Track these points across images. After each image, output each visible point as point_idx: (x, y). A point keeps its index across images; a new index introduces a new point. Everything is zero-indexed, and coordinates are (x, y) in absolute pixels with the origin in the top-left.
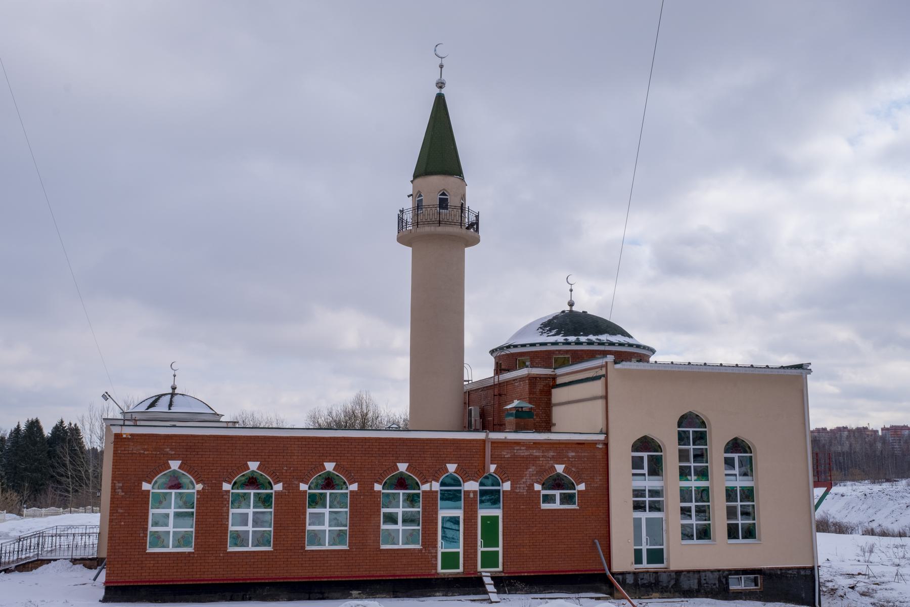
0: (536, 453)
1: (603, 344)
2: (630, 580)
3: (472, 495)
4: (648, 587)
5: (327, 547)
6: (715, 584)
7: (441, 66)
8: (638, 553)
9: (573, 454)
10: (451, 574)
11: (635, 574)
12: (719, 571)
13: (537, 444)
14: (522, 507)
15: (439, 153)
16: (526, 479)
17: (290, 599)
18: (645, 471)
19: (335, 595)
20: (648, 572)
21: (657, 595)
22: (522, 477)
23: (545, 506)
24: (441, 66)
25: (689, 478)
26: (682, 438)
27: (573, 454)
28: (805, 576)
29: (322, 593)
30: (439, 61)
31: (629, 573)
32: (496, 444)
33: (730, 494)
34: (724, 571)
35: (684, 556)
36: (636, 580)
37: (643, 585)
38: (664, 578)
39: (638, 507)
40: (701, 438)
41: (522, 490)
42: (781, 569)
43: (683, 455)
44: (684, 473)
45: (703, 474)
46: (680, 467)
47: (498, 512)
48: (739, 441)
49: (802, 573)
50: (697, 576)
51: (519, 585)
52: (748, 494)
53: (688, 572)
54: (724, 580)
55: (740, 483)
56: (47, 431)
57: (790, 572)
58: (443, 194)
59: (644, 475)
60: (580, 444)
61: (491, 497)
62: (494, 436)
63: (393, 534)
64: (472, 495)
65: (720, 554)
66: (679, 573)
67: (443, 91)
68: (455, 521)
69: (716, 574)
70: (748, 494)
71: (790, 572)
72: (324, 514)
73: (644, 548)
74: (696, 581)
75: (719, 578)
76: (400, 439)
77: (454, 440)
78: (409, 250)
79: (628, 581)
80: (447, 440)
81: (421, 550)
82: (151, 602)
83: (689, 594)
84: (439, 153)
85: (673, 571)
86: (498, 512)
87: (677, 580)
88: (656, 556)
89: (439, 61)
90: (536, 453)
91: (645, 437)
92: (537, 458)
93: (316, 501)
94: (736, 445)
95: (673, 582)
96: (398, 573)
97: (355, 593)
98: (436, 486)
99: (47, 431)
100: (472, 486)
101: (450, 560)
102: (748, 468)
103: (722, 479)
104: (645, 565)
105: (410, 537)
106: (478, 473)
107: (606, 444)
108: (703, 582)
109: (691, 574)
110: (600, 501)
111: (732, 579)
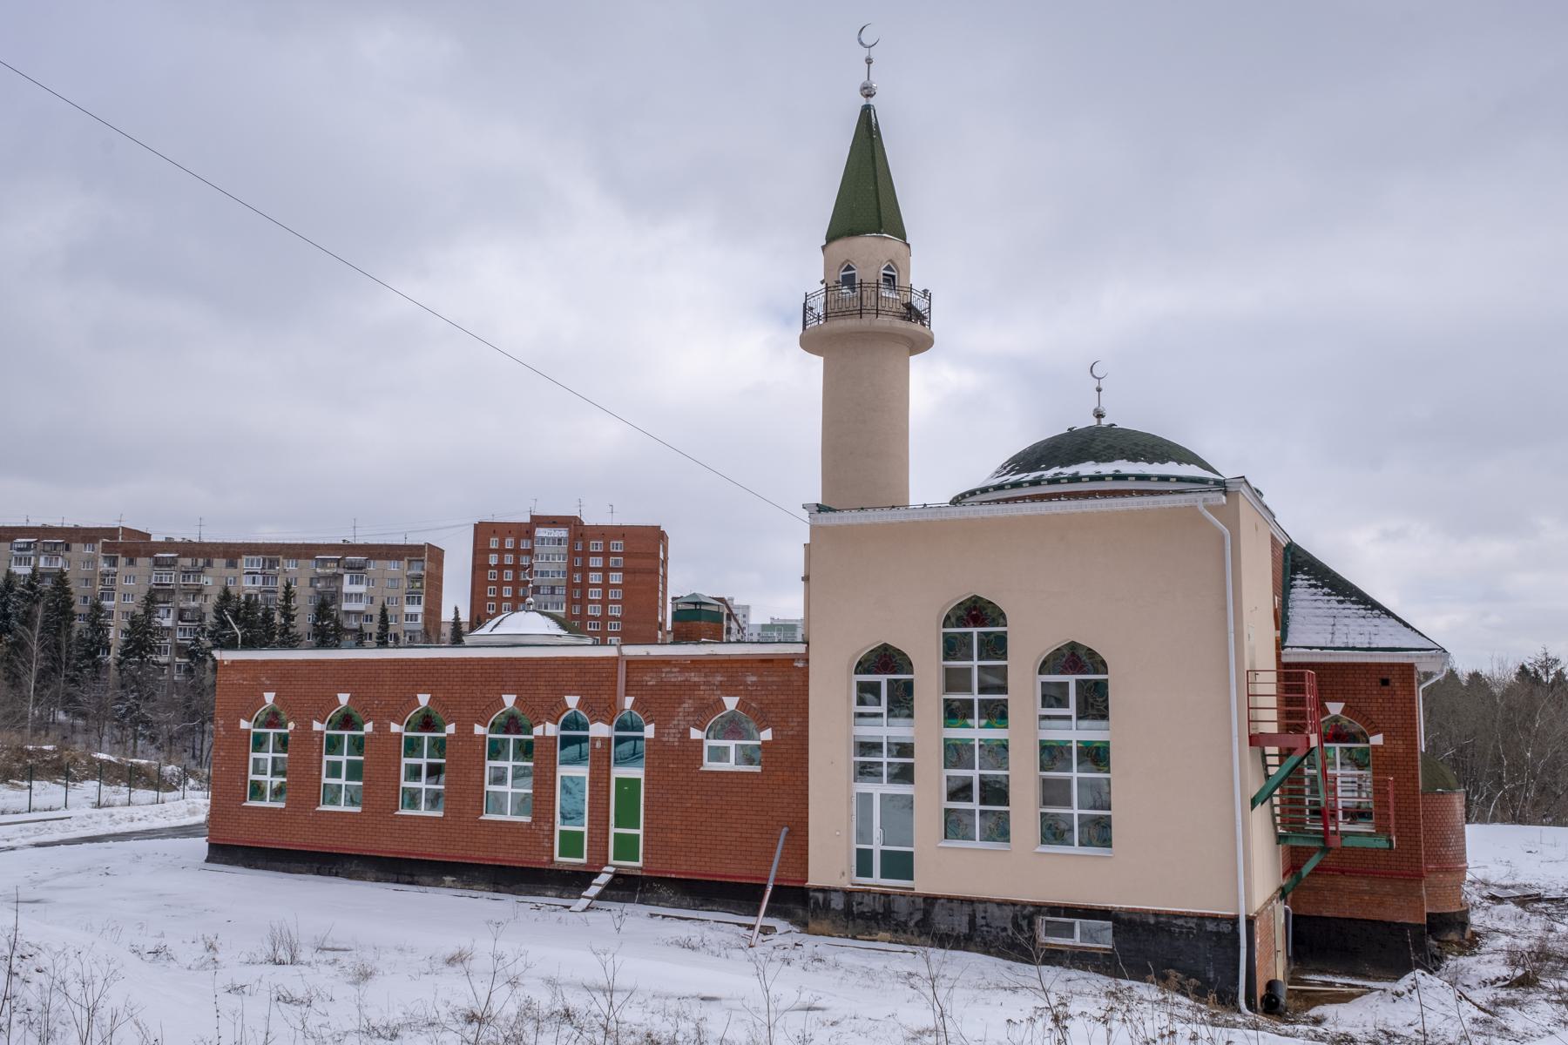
0: (694, 678)
1: (1124, 477)
2: (837, 903)
3: (598, 745)
4: (869, 919)
5: (508, 817)
6: (1005, 929)
7: (869, 61)
8: (864, 859)
9: (754, 679)
10: (569, 864)
11: (848, 894)
12: (1014, 904)
13: (696, 663)
14: (674, 762)
15: (867, 201)
16: (679, 720)
17: (377, 880)
18: (1072, 710)
19: (278, 864)
20: (869, 892)
21: (887, 935)
22: (672, 717)
23: (709, 765)
24: (869, 61)
25: (969, 721)
26: (953, 647)
27: (754, 679)
28: (1218, 934)
29: (412, 875)
30: (864, 53)
31: (835, 890)
32: (632, 663)
33: (1052, 754)
34: (1024, 905)
35: (950, 869)
36: (848, 905)
37: (862, 915)
38: (901, 907)
39: (865, 772)
40: (996, 646)
41: (672, 739)
42: (1157, 914)
43: (954, 680)
44: (955, 713)
45: (997, 713)
46: (946, 700)
47: (637, 772)
48: (1081, 653)
49: (1210, 927)
50: (967, 909)
51: (664, 892)
52: (1096, 756)
53: (950, 899)
54: (1024, 923)
55: (1075, 733)
56: (1464, 679)
57: (1180, 922)
58: (849, 268)
59: (1069, 718)
60: (766, 661)
61: (626, 745)
62: (632, 651)
63: (1049, 836)
64: (598, 745)
65: (1017, 868)
66: (930, 900)
67: (872, 101)
68: (577, 781)
69: (1009, 911)
70: (1096, 756)
71: (1180, 922)
72: (971, 800)
73: (877, 847)
74: (966, 919)
75: (1015, 918)
76: (442, 660)
77: (577, 659)
78: (817, 362)
79: (833, 905)
80: (567, 659)
81: (529, 825)
82: (249, 866)
83: (946, 940)
84: (867, 201)
85: (919, 895)
86: (637, 772)
87: (927, 913)
88: (899, 864)
89: (864, 53)
90: (694, 678)
91: (885, 647)
92: (696, 685)
93: (497, 751)
94: (1073, 658)
95: (918, 916)
96: (501, 856)
97: (448, 879)
98: (552, 730)
99: (1464, 679)
100: (599, 730)
101: (571, 843)
102: (1094, 703)
103: (1027, 727)
104: (876, 880)
105: (521, 804)
106: (606, 711)
107: (806, 658)
108: (980, 921)
109: (955, 905)
110: (788, 762)
111: (1041, 922)
